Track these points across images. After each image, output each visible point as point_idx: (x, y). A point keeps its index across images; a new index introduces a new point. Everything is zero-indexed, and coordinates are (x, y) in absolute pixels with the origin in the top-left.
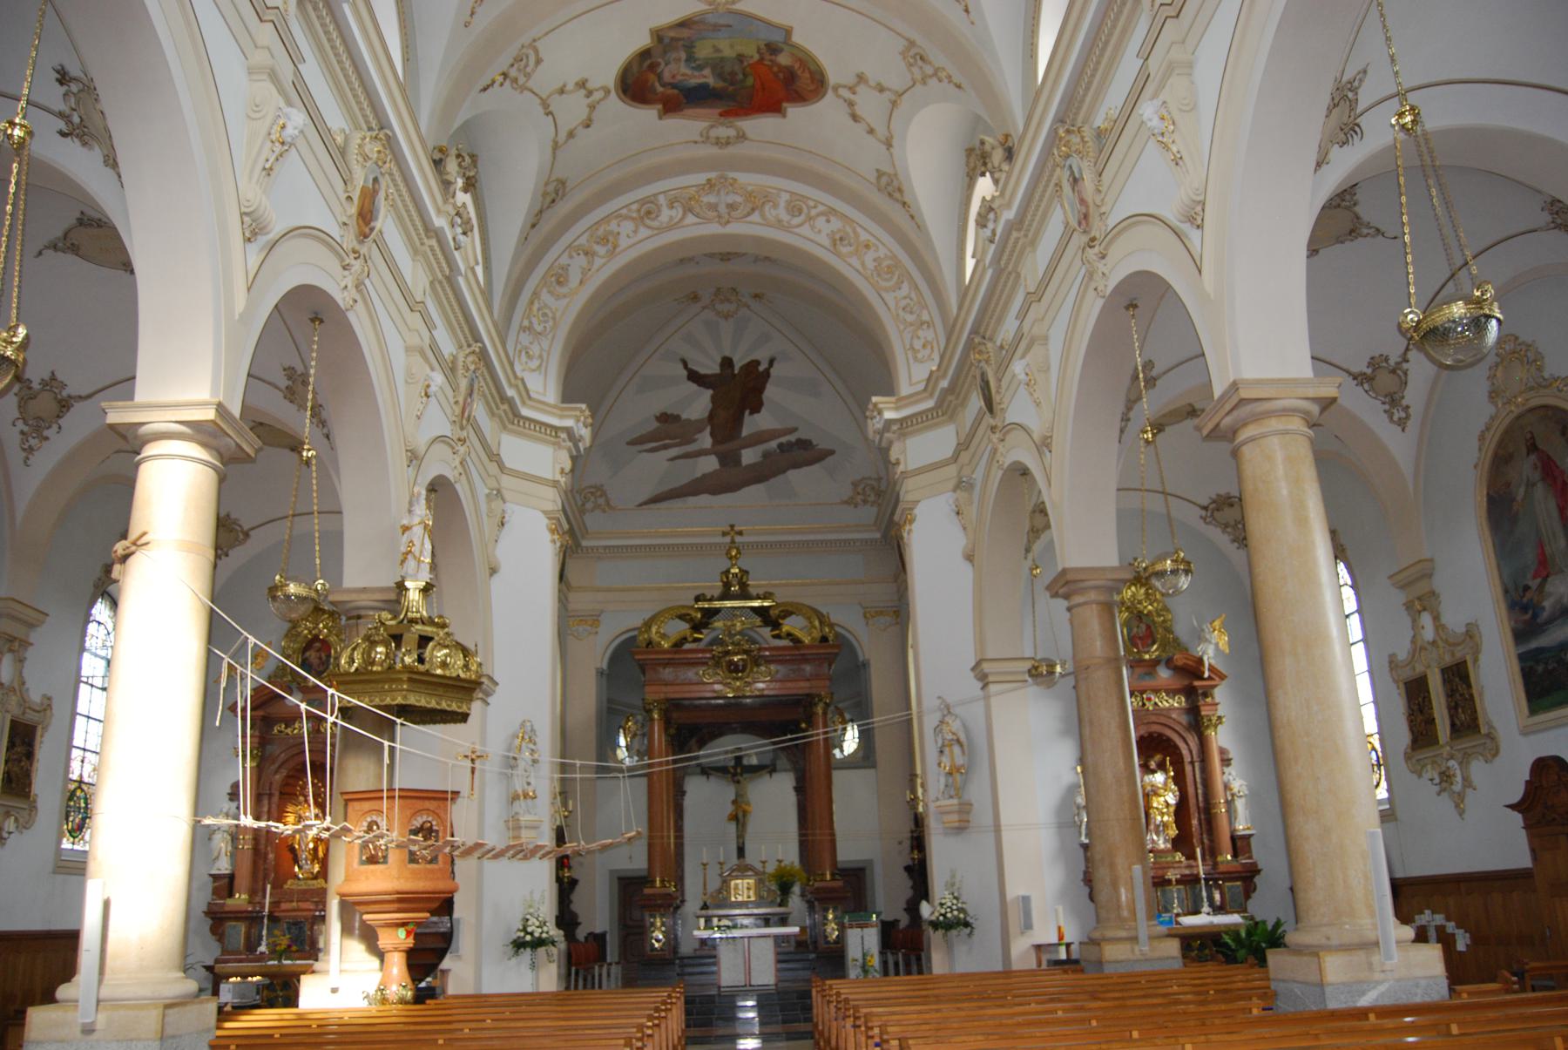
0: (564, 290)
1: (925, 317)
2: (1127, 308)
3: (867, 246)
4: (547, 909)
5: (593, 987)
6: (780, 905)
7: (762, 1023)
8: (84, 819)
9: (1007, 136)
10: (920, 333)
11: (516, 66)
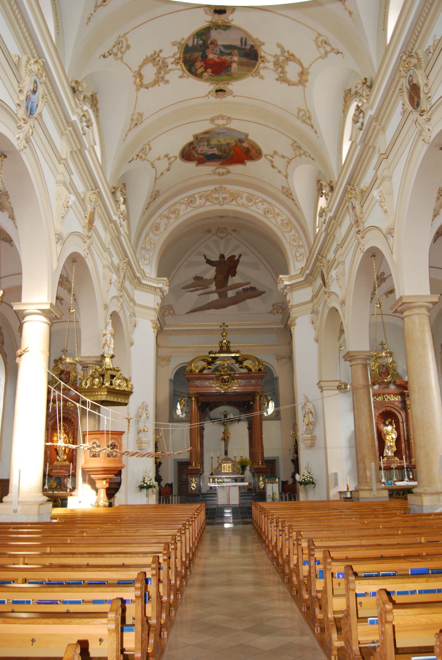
1: (301, 243)
2: (372, 257)
3: (278, 215)
4: (152, 475)
5: (169, 503)
6: (241, 474)
7: (233, 519)
9: (331, 182)
10: (299, 250)
11: (116, 47)
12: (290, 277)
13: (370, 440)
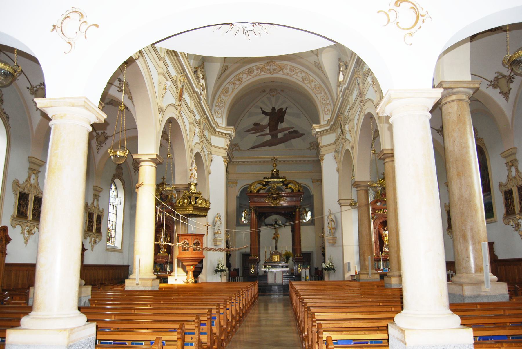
0: (228, 94)
1: (328, 102)
2: (370, 118)
3: (312, 81)
4: (224, 262)
5: (236, 281)
6: (286, 263)
8: (110, 238)
10: (327, 106)
12: (320, 126)
13: (368, 241)
